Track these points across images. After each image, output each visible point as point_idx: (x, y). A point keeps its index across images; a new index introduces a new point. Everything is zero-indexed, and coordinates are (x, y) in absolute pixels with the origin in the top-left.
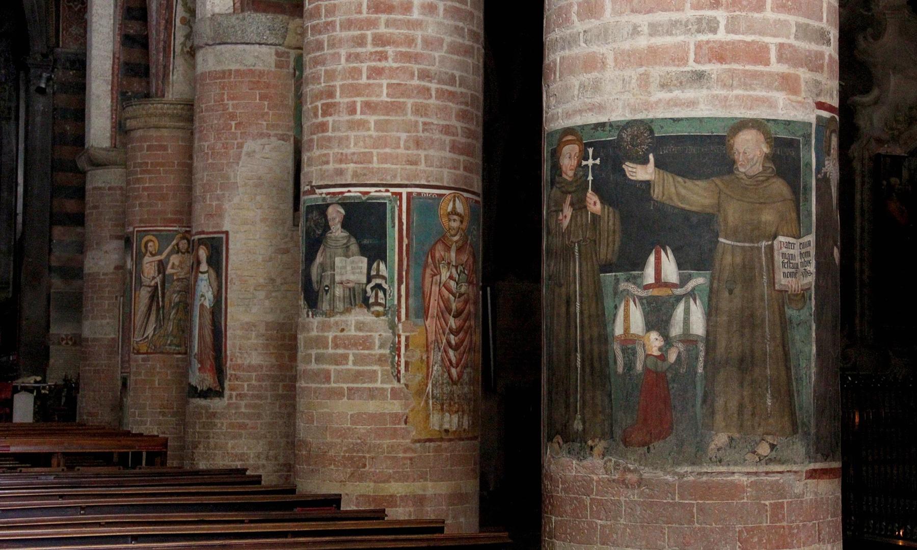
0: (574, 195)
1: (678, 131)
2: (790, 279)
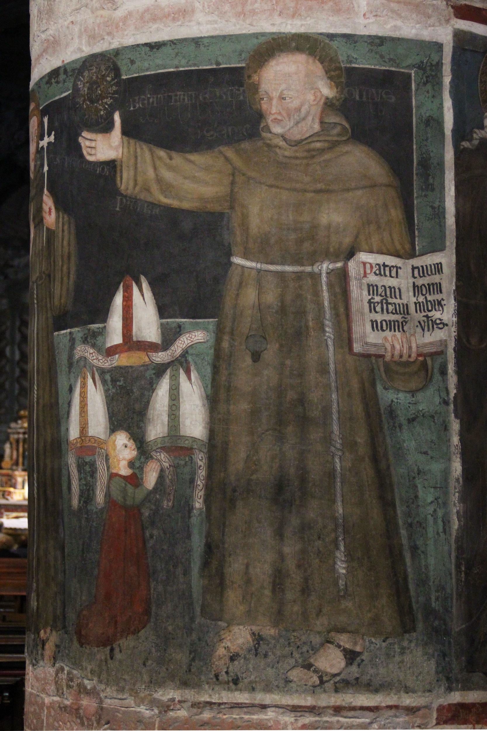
1: (158, 67)
2: (388, 334)
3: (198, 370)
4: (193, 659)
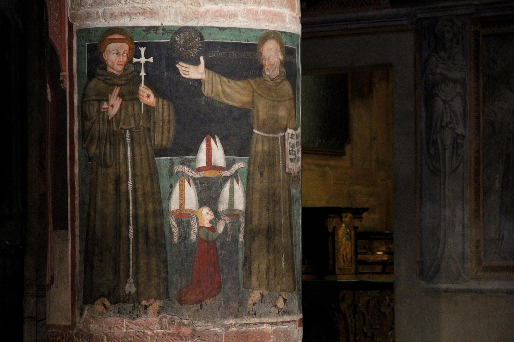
0: (123, 87)
1: (223, 39)
3: (241, 180)
4: (240, 306)
